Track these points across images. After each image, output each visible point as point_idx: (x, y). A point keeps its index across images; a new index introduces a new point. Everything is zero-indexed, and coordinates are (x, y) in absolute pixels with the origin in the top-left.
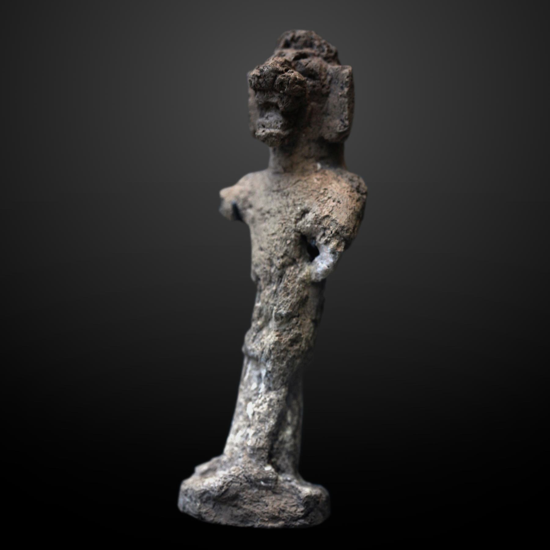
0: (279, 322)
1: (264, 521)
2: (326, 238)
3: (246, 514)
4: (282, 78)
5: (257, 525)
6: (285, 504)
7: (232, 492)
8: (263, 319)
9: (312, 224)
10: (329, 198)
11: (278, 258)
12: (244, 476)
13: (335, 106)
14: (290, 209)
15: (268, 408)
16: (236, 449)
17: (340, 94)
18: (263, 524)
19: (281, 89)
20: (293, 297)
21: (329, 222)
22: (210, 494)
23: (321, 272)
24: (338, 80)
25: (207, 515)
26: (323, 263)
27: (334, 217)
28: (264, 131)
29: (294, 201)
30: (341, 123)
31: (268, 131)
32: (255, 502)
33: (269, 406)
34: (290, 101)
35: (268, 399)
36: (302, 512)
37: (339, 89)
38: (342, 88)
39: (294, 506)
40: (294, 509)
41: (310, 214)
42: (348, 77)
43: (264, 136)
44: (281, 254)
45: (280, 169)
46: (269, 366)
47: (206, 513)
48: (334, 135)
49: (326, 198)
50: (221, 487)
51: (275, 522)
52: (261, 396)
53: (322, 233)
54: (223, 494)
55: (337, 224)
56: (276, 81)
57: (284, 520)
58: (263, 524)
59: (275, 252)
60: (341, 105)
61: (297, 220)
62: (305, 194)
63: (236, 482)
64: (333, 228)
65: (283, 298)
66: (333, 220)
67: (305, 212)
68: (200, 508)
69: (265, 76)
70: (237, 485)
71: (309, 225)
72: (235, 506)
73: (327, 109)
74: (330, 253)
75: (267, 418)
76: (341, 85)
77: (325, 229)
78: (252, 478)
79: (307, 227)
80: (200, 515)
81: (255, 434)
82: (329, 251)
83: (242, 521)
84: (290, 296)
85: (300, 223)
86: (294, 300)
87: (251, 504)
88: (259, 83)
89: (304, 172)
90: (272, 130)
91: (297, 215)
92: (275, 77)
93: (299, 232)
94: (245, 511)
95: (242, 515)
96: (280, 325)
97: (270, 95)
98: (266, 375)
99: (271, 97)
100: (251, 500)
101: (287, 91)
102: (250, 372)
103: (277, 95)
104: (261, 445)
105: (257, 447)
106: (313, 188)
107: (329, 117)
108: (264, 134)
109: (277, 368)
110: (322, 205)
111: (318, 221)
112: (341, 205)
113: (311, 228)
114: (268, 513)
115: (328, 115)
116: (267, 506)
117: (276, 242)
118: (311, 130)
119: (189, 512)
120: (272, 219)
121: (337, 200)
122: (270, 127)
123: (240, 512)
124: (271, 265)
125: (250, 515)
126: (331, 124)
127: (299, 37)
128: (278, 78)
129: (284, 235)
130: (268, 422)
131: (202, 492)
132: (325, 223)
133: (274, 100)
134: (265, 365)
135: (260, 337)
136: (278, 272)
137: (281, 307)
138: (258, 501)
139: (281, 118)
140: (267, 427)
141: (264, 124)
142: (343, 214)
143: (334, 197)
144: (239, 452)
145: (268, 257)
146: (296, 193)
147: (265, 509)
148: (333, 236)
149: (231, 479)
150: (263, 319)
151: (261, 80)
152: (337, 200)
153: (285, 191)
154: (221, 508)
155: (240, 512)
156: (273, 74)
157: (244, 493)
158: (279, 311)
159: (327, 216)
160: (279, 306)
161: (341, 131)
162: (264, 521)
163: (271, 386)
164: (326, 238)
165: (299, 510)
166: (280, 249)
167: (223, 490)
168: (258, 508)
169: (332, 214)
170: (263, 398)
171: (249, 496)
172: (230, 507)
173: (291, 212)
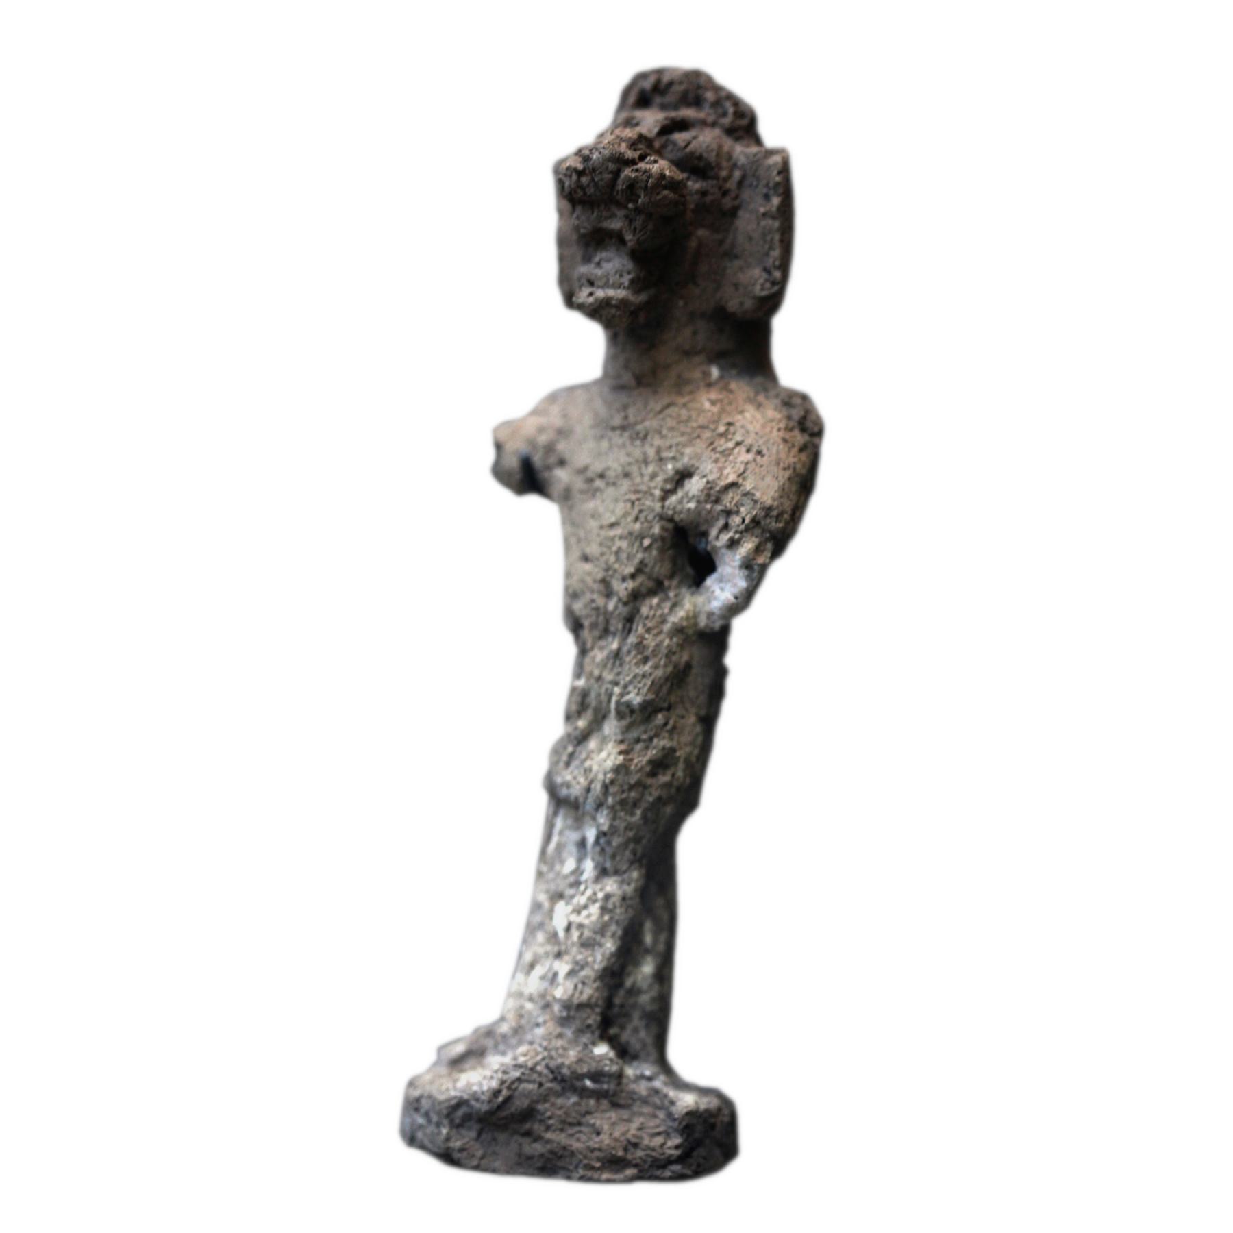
0: (624, 723)
1: (593, 1168)
2: (731, 534)
3: (552, 1152)
4: (633, 175)
6: (640, 1129)
7: (521, 1103)
8: (589, 714)
9: (698, 502)
10: (738, 444)
11: (624, 579)
12: (547, 1066)
13: (750, 239)
14: (651, 469)
15: (602, 915)
16: (529, 1006)
17: (762, 210)
19: (630, 201)
20: (656, 667)
21: (737, 498)
22: (472, 1107)
23: (721, 609)
24: (758, 179)
25: (465, 1154)
27: (748, 486)
28: (591, 294)
29: (658, 451)
30: (765, 275)
31: (600, 294)
32: (571, 1125)
33: (604, 909)
34: (650, 227)
35: (600, 895)
36: (677, 1147)
37: (759, 200)
38: (767, 197)
39: (659, 1134)
40: (658, 1140)
41: (695, 479)
43: (591, 304)
44: (630, 569)
45: (627, 378)
46: (603, 819)
47: (461, 1150)
48: (749, 304)
49: (730, 445)
50: (496, 1093)
52: (586, 889)
53: (721, 522)
54: (500, 1107)
55: (756, 502)
56: (620, 181)
57: (636, 1166)
59: (616, 566)
60: (764, 235)
61: (666, 494)
62: (683, 434)
63: (529, 1081)
64: (747, 511)
65: (633, 668)
66: (746, 494)
67: (683, 476)
68: (448, 1139)
69: (594, 170)
70: (530, 1086)
71: (692, 505)
72: (528, 1134)
73: (733, 245)
74: (741, 567)
75: (598, 937)
76: (765, 191)
77: (728, 513)
78: (565, 1071)
79: (689, 509)
81: (571, 973)
82: (737, 563)
84: (650, 664)
85: (673, 499)
86: (659, 673)
87: (562, 1130)
89: (681, 385)
90: (611, 293)
91: (666, 481)
92: (617, 173)
93: (671, 520)
94: (549, 1147)
95: (542, 1155)
96: (628, 729)
97: (604, 214)
98: (597, 842)
99: (607, 218)
100: (563, 1122)
101: (643, 204)
103: (621, 213)
104: (585, 997)
105: (576, 1001)
106: (702, 421)
107: (737, 263)
108: (591, 300)
109: (621, 825)
110: (723, 460)
111: (713, 494)
112: (764, 460)
113: (698, 512)
114: (600, 1150)
115: (736, 257)
116: (598, 1134)
117: (618, 543)
118: (697, 291)
120: (611, 491)
121: (755, 449)
122: (606, 285)
123: (538, 1148)
124: (609, 594)
126: (743, 278)
127: (671, 84)
128: (622, 176)
129: (637, 526)
130: (600, 945)
131: (453, 1102)
132: (729, 500)
133: (615, 224)
134: (594, 819)
135: (583, 755)
136: (624, 610)
137: (630, 688)
138: (579, 1124)
139: (629, 265)
140: (599, 957)
141: (592, 278)
142: (768, 479)
143: (748, 441)
144: (535, 1014)
145: (600, 576)
146: (664, 432)
147: (595, 1142)
148: (747, 529)
149: (517, 1074)
150: (589, 714)
151: (584, 180)
152: (755, 449)
153: (639, 427)
154: (494, 1139)
155: (538, 1148)
156: (611, 166)
157: (547, 1105)
158: (626, 698)
159: (734, 485)
160: (625, 687)
161: (764, 293)
163: (608, 865)
164: (731, 534)
165: (670, 1143)
166: (628, 558)
167: (501, 1099)
168: (578, 1140)
169: (744, 479)
170: (589, 892)
171: (559, 1113)
172: (517, 1137)
173: (653, 476)
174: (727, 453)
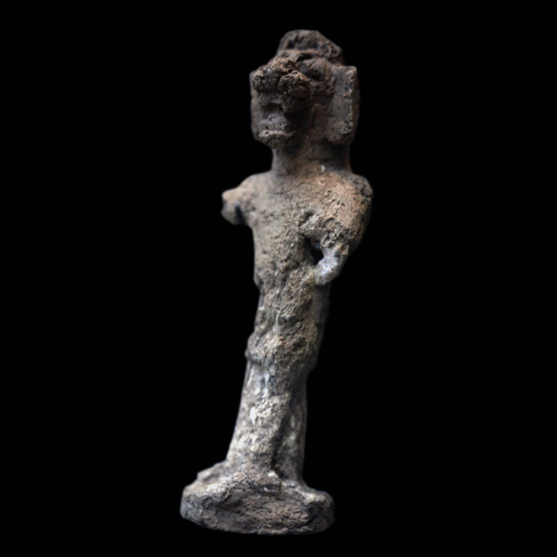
0: (282, 326)
1: (268, 528)
2: (330, 241)
3: (249, 520)
4: (286, 79)
5: (260, 532)
6: (289, 510)
7: (235, 498)
8: (266, 323)
9: (316, 227)
10: (333, 200)
11: (282, 262)
12: (247, 482)
13: (339, 108)
14: (294, 212)
15: (272, 413)
16: (239, 454)
17: (344, 95)
18: (266, 530)
19: (284, 91)
20: (296, 301)
21: (333, 225)
22: (213, 500)
23: (325, 275)
24: (342, 81)
25: (210, 521)
26: (328, 266)
27: (338, 219)
28: (267, 133)
29: (297, 204)
30: (345, 124)
31: (271, 133)
32: (258, 508)
33: (273, 411)
34: (294, 102)
35: (271, 404)
36: (306, 518)
37: (343, 90)
38: (346, 89)
39: (298, 512)
40: (297, 515)
41: (314, 216)
42: (352, 78)
43: (267, 137)
44: (285, 257)
46: (272, 370)
47: (208, 519)
48: (338, 137)
49: (330, 201)
50: (224, 494)
51: (279, 529)
52: (265, 401)
53: (326, 236)
54: (226, 500)
55: (341, 227)
56: (280, 82)
57: (287, 527)
58: (266, 530)
59: (278, 256)
60: (345, 106)
61: (301, 223)
62: (308, 196)
63: (239, 489)
64: (338, 231)
65: (286, 302)
66: (337, 223)
67: (309, 215)
68: (202, 515)
69: (268, 77)
70: (240, 491)
71: (313, 228)
72: (238, 512)
73: (331, 111)
74: (335, 256)
75: (270, 424)
76: (345, 86)
77: (329, 232)
78: (255, 484)
79: (311, 230)
80: (202, 521)
81: (258, 440)
82: (333, 254)
83: (245, 528)
84: (294, 300)
85: (304, 226)
87: (254, 510)
88: (262, 84)
89: (308, 174)
90: (276, 132)
91: (301, 217)
92: (279, 78)
93: (303, 235)
94: (248, 518)
95: (245, 522)
96: (284, 329)
97: (273, 97)
98: (270, 380)
99: (274, 99)
100: (254, 507)
101: (291, 92)
102: (253, 376)
103: (280, 96)
104: (264, 450)
105: (260, 452)
106: (317, 190)
107: (333, 119)
108: (267, 135)
109: (280, 373)
110: (327, 208)
111: (322, 223)
112: (345, 208)
113: (315, 231)
114: (271, 519)
115: (333, 116)
116: (270, 512)
117: (279, 245)
118: (315, 132)
119: (191, 518)
120: (276, 222)
121: (341, 203)
122: (274, 129)
123: (243, 518)
124: (275, 268)
125: (253, 522)
126: (336, 125)
127: (303, 38)
128: (281, 79)
129: (288, 238)
130: (271, 427)
131: (205, 498)
132: (329, 226)
133: (278, 101)
134: (268, 370)
135: (264, 341)
136: (282, 276)
137: (285, 311)
138: (262, 508)
139: (284, 120)
140: (271, 432)
141: (268, 126)
142: (347, 216)
143: (338, 199)
144: (242, 458)
145: (271, 260)
146: (300, 195)
147: (269, 516)
148: (338, 239)
149: (234, 485)
150: (266, 323)
151: (264, 81)
152: (341, 203)
153: (289, 193)
154: (223, 515)
155: (243, 518)
156: (276, 75)
157: (247, 499)
158: (283, 315)
159: (331, 219)
160: (283, 310)
161: (345, 132)
162: (268, 528)
163: (275, 391)
164: (330, 241)
165: (302, 517)
166: (284, 252)
167: (226, 496)
168: (261, 515)
169: (336, 216)
170: (266, 403)
171: (253, 503)
172: (233, 514)
173: (295, 215)
174: (328, 205)
